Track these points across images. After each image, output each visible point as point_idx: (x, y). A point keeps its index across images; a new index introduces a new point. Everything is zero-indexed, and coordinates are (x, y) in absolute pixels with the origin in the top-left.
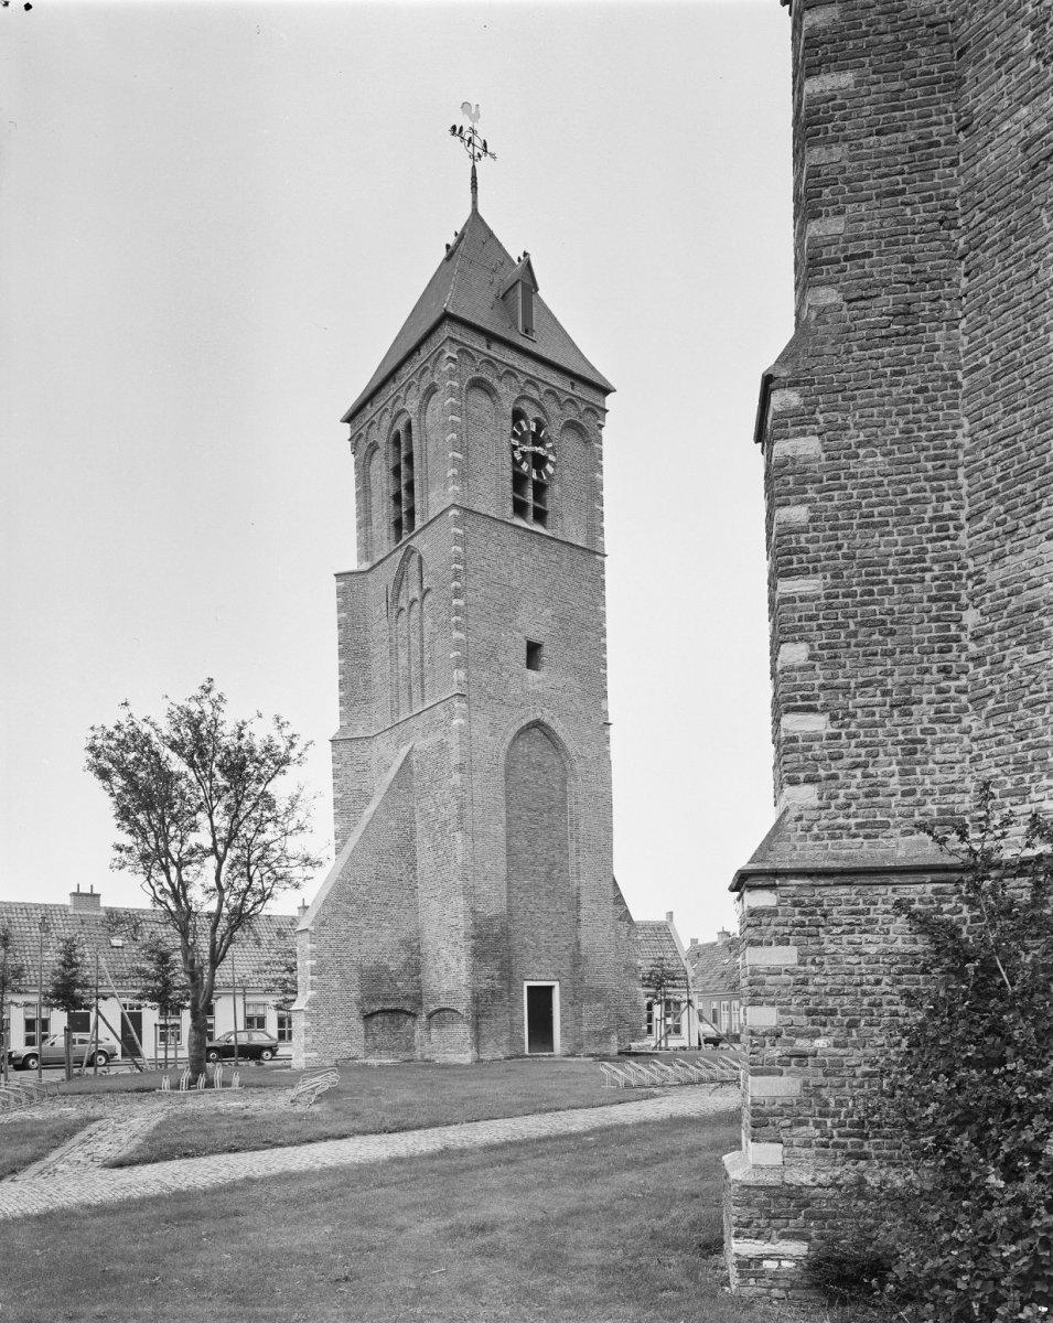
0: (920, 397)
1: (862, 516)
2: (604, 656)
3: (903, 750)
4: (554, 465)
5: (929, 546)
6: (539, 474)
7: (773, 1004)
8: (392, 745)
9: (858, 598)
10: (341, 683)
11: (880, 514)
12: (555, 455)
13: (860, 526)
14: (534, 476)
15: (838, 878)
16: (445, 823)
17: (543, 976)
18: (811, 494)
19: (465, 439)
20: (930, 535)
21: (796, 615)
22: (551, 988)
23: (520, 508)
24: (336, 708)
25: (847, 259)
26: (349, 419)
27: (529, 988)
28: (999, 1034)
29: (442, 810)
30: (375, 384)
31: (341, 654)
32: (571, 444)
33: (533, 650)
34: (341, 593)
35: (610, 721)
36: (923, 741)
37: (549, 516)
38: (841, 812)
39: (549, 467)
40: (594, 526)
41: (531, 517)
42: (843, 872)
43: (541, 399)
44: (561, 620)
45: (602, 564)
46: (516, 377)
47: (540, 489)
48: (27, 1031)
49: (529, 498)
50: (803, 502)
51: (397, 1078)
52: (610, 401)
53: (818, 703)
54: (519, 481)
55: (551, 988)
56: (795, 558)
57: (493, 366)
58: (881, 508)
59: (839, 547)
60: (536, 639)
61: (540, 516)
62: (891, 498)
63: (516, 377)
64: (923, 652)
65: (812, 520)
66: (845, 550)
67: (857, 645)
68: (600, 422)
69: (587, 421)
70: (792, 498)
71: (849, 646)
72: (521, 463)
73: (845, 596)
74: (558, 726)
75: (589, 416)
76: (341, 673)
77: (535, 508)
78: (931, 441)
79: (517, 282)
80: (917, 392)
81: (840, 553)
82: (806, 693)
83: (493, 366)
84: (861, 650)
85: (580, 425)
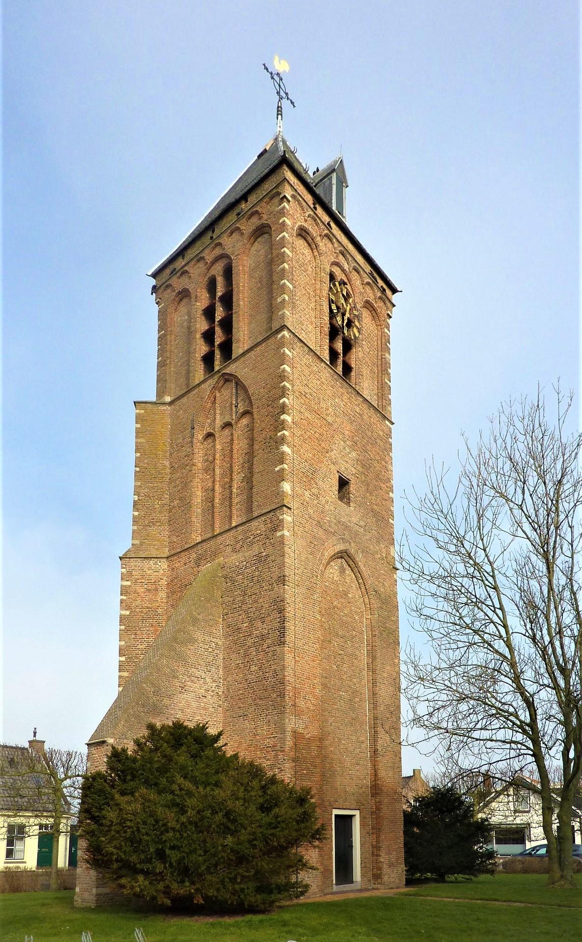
8: (192, 564)
10: (138, 432)
16: (263, 637)
17: (347, 804)
24: (130, 527)
26: (155, 275)
28: (209, 784)
30: (214, 217)
31: (138, 476)
32: (366, 321)
33: (343, 483)
34: (139, 419)
37: (353, 374)
40: (383, 390)
44: (363, 466)
51: (212, 925)
52: (395, 298)
54: (334, 332)
55: (351, 817)
57: (317, 224)
60: (346, 475)
63: (333, 244)
74: (359, 557)
76: (136, 493)
79: (334, 170)
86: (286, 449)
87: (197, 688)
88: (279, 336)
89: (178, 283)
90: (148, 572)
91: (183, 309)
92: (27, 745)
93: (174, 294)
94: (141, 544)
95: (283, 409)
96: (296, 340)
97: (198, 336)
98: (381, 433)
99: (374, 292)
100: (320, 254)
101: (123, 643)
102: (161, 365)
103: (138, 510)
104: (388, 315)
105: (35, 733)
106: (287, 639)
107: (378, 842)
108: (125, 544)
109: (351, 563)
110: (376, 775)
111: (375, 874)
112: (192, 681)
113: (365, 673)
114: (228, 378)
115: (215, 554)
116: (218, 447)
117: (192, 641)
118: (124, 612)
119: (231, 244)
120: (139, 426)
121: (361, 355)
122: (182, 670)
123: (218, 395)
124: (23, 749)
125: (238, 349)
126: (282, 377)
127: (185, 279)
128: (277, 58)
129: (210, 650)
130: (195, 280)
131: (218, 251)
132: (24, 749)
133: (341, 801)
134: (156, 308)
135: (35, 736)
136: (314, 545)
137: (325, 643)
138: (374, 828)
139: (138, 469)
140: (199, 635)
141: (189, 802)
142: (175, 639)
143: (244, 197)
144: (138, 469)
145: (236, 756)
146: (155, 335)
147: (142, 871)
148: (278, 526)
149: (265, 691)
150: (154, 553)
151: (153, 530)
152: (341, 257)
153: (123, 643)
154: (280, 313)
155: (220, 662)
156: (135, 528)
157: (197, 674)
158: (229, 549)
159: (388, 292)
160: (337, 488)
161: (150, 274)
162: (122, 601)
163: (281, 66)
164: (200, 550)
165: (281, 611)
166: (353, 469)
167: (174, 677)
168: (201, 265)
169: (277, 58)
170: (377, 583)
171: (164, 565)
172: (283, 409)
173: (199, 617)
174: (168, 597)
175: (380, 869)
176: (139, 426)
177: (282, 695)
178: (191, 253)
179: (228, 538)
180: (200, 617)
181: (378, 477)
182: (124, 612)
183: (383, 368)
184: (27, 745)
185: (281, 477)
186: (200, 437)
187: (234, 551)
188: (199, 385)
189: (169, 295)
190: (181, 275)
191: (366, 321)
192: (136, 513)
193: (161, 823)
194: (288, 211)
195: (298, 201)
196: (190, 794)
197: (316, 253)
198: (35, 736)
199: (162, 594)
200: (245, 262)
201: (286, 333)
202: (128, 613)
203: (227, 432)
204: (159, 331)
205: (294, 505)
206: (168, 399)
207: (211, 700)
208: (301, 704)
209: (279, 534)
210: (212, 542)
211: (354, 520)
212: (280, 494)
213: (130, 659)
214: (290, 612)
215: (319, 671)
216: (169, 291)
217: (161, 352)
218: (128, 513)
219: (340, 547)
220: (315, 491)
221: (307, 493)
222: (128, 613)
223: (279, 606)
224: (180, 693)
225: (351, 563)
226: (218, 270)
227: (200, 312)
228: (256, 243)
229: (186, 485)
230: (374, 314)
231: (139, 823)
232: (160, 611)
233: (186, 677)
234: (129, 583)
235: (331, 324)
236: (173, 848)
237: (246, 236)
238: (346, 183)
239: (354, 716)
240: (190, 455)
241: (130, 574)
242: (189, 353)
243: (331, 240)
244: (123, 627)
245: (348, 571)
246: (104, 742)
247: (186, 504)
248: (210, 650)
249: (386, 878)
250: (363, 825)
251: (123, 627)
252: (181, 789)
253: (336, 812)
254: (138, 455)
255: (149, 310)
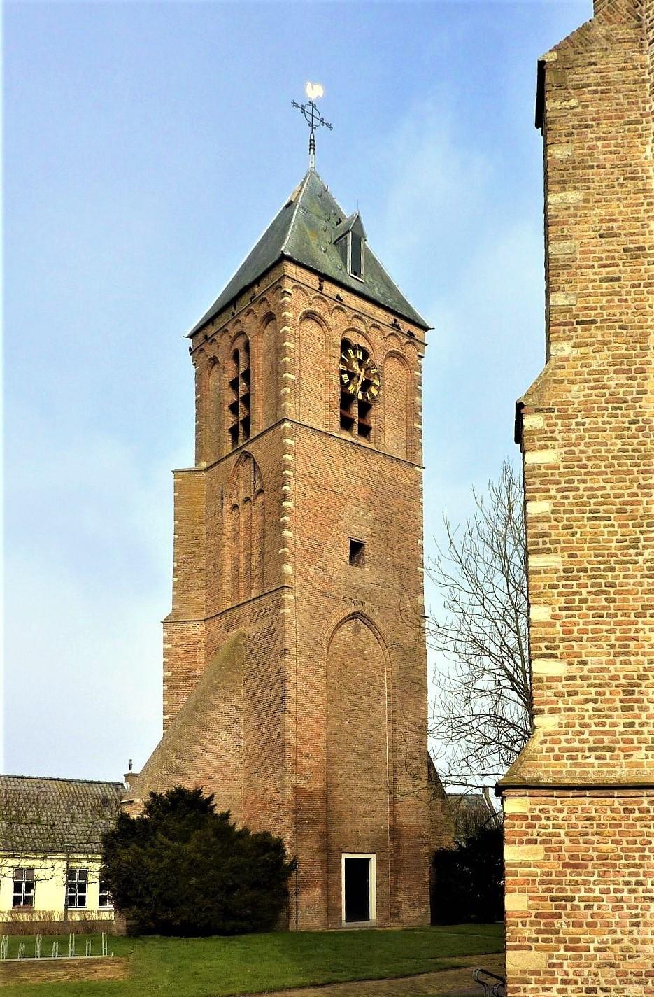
0: (633, 427)
1: (591, 512)
2: (421, 556)
3: (624, 691)
4: (378, 388)
5: (641, 537)
6: (363, 395)
7: (522, 891)
9: (589, 573)
10: (176, 499)
11: (605, 511)
12: (379, 380)
13: (590, 519)
14: (360, 397)
15: (575, 791)
16: (271, 703)
17: (360, 849)
18: (553, 493)
19: (297, 362)
20: (642, 529)
21: (542, 584)
22: (368, 860)
23: (346, 424)
25: (578, 323)
26: (192, 336)
27: (347, 860)
29: (268, 691)
31: (177, 543)
32: (392, 370)
33: (356, 548)
34: (177, 487)
35: (426, 615)
36: (639, 685)
37: (372, 432)
38: (577, 738)
39: (373, 390)
40: (413, 439)
41: (356, 432)
42: (579, 788)
43: (368, 332)
44: (383, 523)
45: (421, 475)
46: (345, 312)
47: (365, 408)
48: (14, 893)
49: (355, 410)
50: (546, 498)
52: (427, 337)
53: (558, 652)
54: (346, 400)
55: (368, 860)
56: (541, 540)
57: (325, 301)
58: (605, 507)
59: (574, 534)
60: (358, 539)
61: (365, 431)
62: (612, 499)
63: (345, 312)
64: (637, 616)
65: (553, 512)
66: (578, 536)
67: (588, 609)
68: (420, 354)
69: (409, 351)
70: (538, 495)
71: (581, 609)
72: (348, 385)
73: (579, 571)
74: (376, 616)
75: (410, 348)
77: (360, 425)
78: (642, 460)
79: (348, 232)
80: (630, 423)
81: (574, 538)
82: (550, 644)
83: (325, 301)
84: (591, 613)
85: (402, 356)
86: (287, 533)
87: (219, 749)
88: (282, 427)
89: (211, 350)
90: (187, 635)
91: (215, 374)
92: (122, 780)
93: (207, 359)
94: (181, 608)
95: (285, 496)
96: (299, 427)
97: (226, 408)
98: (408, 482)
99: (399, 339)
100: (329, 329)
101: (166, 702)
102: (199, 429)
103: (177, 576)
104: (419, 356)
105: (131, 766)
106: (288, 706)
107: (396, 883)
108: (167, 608)
109: (366, 621)
110: (395, 820)
111: (391, 910)
112: (213, 744)
113: (385, 723)
114: (248, 456)
115: (239, 622)
116: (242, 519)
117: (212, 707)
118: (166, 674)
119: (250, 324)
120: (177, 494)
121: (380, 411)
122: (202, 735)
123: (241, 469)
124: (116, 785)
125: (255, 430)
126: (284, 466)
127: (213, 346)
128: (309, 85)
129: (231, 713)
130: (221, 349)
131: (238, 328)
132: (118, 784)
133: (352, 846)
134: (193, 370)
135: (130, 769)
136: (318, 615)
137: (329, 704)
138: (392, 868)
139: (177, 536)
140: (219, 702)
141: (166, 853)
142: (195, 708)
143: (256, 282)
144: (177, 536)
145: (226, 816)
146: (193, 398)
147: (135, 903)
148: (280, 605)
149: (271, 752)
150: (192, 616)
151: (192, 595)
152: (356, 320)
153: (166, 702)
154: (283, 405)
155: (241, 723)
156: (175, 593)
157: (218, 736)
158: (248, 619)
159: (417, 332)
160: (348, 554)
161: (187, 335)
162: (164, 664)
163: (314, 92)
164: (228, 616)
165: (283, 681)
166: (368, 530)
167: (195, 741)
168: (226, 336)
169: (309, 85)
170: (398, 635)
171: (202, 627)
172: (285, 496)
173: (219, 685)
174: (205, 658)
175: (398, 908)
176: (177, 494)
177: (283, 756)
178: (219, 323)
179: (246, 610)
180: (221, 685)
181: (402, 529)
182: (166, 674)
183: (414, 413)
184: (122, 780)
185: (282, 560)
186: (229, 507)
187: (252, 622)
188: (226, 457)
189: (203, 359)
190: (211, 342)
191: (392, 370)
192: (176, 579)
193: (145, 869)
194: (289, 303)
195: (301, 288)
196: (168, 847)
197: (326, 329)
198: (130, 769)
199: (201, 655)
200: (259, 345)
201: (287, 425)
202: (170, 674)
203: (248, 505)
204: (196, 394)
205: (296, 583)
206: (204, 465)
207: (232, 758)
208: (304, 762)
209: (281, 611)
210: (237, 611)
211: (370, 579)
212: (281, 575)
213: (172, 718)
214: (291, 681)
215: (324, 730)
216: (203, 354)
217: (199, 416)
218: (169, 579)
219: (354, 609)
220: (321, 564)
221: (311, 569)
222: (170, 674)
223: (282, 677)
224: (202, 754)
225: (366, 621)
226: (239, 345)
227: (227, 384)
228: (268, 327)
229: (218, 552)
230: (402, 360)
231: (131, 869)
232: (198, 671)
233: (206, 740)
234: (170, 646)
235: (342, 393)
236: (155, 886)
237: (259, 319)
238: (364, 237)
239: (369, 765)
240: (221, 523)
241: (171, 636)
242: (220, 424)
243: (342, 310)
244: (166, 688)
245: (364, 629)
246: (132, 802)
247: (218, 572)
248: (231, 713)
249: (404, 917)
250: (379, 867)
251: (166, 688)
252: (162, 844)
253: (345, 856)
254: (177, 522)
255: (187, 370)
